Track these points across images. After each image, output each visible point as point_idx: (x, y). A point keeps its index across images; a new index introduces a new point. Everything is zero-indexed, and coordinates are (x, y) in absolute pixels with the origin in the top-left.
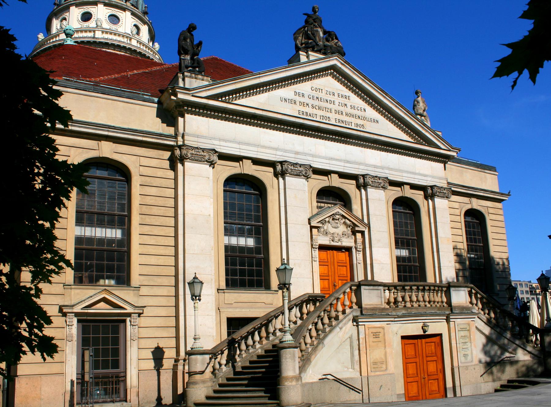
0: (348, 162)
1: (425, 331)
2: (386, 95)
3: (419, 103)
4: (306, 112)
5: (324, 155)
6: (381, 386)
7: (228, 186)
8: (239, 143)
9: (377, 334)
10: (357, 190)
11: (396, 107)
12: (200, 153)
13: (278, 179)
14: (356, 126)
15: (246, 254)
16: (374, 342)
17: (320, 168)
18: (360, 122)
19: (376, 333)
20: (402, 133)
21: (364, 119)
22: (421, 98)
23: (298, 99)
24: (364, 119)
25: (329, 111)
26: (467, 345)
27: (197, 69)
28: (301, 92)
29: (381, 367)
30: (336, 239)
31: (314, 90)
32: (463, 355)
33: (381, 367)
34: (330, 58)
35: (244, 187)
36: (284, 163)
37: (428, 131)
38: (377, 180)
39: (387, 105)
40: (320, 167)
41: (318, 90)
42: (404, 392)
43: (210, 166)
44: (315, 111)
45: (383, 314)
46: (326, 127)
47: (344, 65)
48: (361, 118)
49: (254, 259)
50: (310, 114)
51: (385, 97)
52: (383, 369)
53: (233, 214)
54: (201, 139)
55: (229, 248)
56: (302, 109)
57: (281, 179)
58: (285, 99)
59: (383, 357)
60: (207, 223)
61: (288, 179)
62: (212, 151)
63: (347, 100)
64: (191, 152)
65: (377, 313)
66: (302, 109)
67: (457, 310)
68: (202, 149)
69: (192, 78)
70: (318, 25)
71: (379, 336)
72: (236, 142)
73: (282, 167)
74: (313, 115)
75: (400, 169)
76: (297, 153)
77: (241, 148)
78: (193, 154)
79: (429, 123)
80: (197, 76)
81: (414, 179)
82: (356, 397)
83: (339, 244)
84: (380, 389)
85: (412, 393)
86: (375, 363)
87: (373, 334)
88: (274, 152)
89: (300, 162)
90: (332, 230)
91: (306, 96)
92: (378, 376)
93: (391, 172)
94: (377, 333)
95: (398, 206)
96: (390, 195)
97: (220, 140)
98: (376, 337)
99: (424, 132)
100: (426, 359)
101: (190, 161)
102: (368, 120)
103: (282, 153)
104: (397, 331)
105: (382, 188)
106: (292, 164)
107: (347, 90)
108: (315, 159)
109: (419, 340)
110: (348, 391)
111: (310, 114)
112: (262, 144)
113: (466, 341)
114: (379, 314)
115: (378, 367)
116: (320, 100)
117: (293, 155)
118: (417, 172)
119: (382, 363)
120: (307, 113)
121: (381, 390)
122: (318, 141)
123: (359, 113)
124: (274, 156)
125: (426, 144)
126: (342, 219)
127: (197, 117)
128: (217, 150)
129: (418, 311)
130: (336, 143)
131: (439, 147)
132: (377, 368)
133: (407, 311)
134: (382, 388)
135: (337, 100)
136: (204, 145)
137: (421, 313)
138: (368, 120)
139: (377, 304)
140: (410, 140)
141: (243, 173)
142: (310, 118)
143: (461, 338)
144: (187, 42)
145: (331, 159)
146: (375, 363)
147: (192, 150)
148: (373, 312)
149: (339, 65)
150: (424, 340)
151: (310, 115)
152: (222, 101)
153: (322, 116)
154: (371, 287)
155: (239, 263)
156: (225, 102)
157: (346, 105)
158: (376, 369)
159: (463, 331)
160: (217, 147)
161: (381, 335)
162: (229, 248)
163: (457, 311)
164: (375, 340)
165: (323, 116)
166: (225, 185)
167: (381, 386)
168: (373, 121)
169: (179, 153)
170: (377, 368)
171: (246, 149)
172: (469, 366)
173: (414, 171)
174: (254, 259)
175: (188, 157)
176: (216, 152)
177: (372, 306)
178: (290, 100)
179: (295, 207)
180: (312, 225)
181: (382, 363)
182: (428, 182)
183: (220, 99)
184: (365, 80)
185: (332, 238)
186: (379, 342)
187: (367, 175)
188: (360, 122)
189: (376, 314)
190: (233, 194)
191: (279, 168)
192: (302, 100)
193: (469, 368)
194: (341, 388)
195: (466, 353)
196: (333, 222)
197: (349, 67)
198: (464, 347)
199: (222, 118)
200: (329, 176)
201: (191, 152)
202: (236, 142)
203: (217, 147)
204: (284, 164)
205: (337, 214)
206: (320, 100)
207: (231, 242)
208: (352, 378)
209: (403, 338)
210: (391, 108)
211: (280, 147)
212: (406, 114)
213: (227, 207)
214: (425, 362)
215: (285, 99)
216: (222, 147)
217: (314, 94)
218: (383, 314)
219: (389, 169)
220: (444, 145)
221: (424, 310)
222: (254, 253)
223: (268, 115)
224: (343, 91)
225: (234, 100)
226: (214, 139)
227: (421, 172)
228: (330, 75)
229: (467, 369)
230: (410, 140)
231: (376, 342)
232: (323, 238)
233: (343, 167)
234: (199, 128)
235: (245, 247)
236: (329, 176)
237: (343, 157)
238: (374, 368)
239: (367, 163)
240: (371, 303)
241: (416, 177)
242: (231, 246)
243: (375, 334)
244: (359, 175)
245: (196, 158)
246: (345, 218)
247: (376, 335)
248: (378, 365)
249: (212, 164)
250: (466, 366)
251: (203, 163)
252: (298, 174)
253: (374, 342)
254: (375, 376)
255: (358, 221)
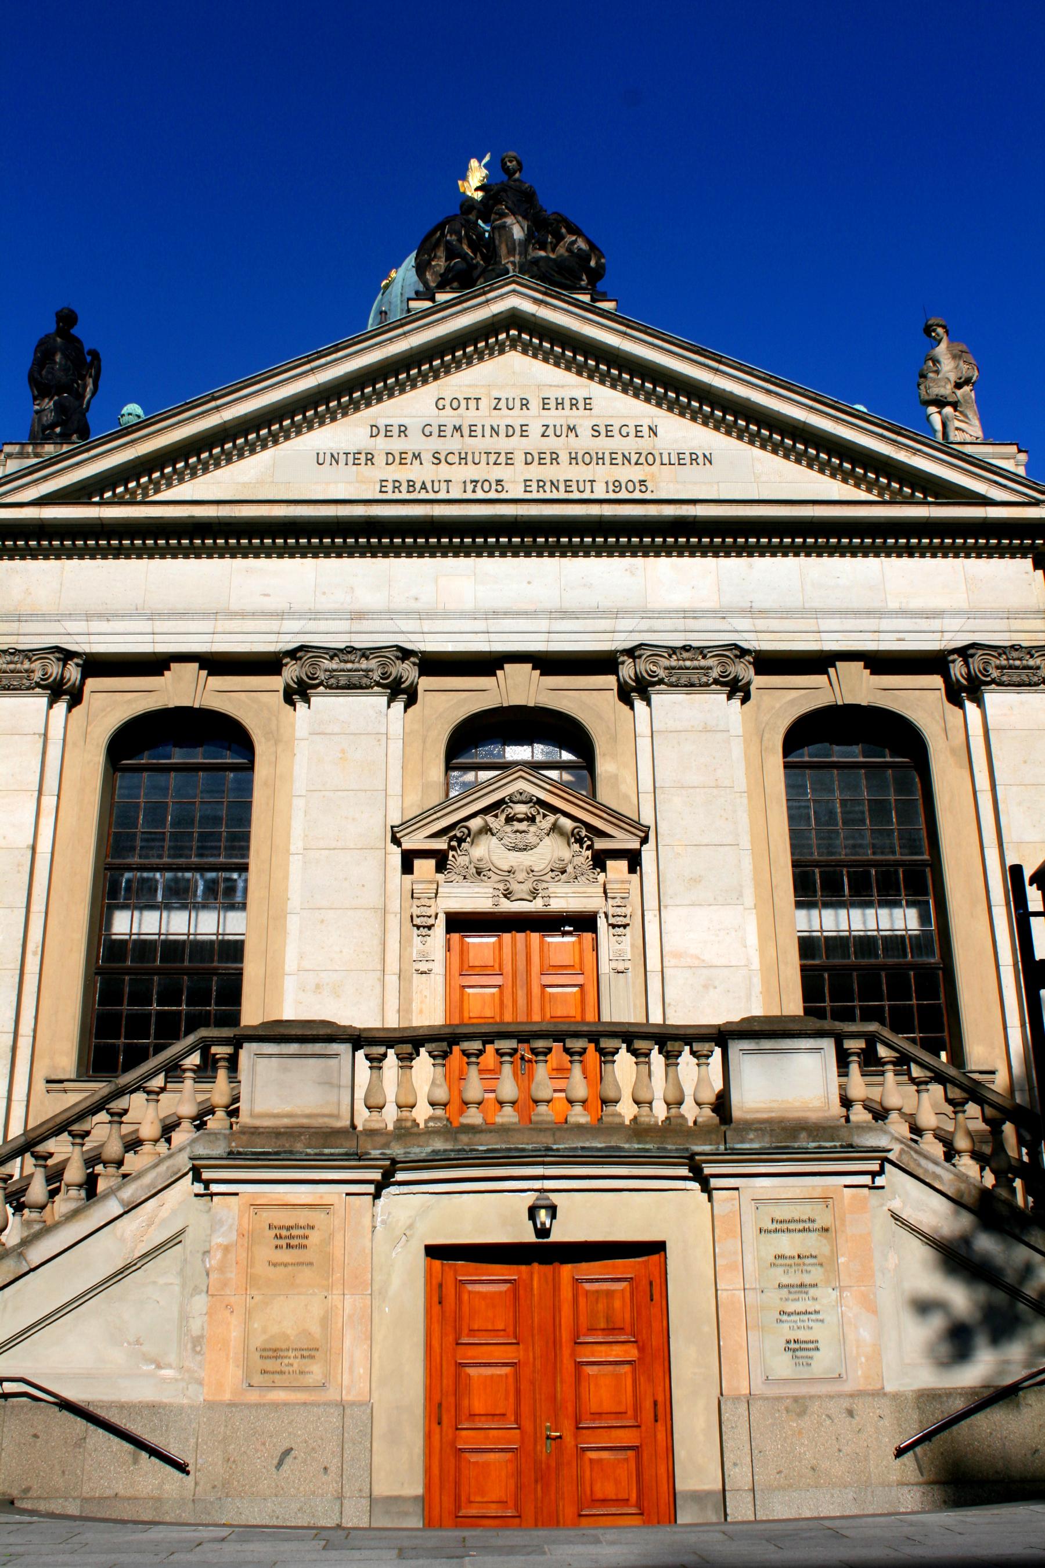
0: (565, 614)
1: (543, 1232)
2: (720, 362)
3: (938, 362)
4: (408, 481)
5: (469, 606)
6: (288, 1452)
7: (146, 753)
8: (152, 617)
9: (294, 1232)
10: (949, 707)
11: (769, 392)
12: (1024, 662)
13: (961, 705)
14: (611, 487)
15: (186, 964)
16: (275, 1265)
17: (450, 649)
18: (636, 473)
19: (288, 1228)
20: (814, 475)
21: (648, 458)
22: (951, 340)
23: (381, 444)
24: (648, 458)
25: (502, 459)
26: (815, 1299)
27: (58, 430)
28: (395, 422)
29: (301, 1373)
30: (521, 889)
31: (448, 407)
32: (784, 1345)
33: (301, 1373)
34: (485, 293)
35: (200, 750)
36: (971, 651)
37: (919, 450)
38: (1020, 659)
39: (731, 393)
40: (450, 647)
41: (463, 403)
42: (419, 1490)
43: (729, 698)
44: (444, 471)
45: (327, 1151)
46: (313, 514)
47: (546, 304)
48: (633, 461)
49: (215, 978)
50: (423, 483)
51: (717, 370)
52: (309, 1380)
53: (153, 840)
54: (30, 623)
55: (130, 946)
56: (396, 473)
57: (970, 707)
58: (332, 456)
59: (315, 1329)
60: (19, 872)
61: (992, 698)
62: (731, 650)
63: (582, 412)
64: (998, 662)
65: (299, 1147)
66: (396, 473)
67: (751, 1136)
68: (24, 651)
69: (28, 458)
70: (507, 207)
71: (304, 1242)
72: (140, 615)
73: (967, 664)
74: (436, 484)
75: (807, 606)
76: (358, 615)
77: (156, 630)
78: (673, 668)
79: (976, 422)
80: (39, 450)
81: (875, 636)
82: (167, 1487)
83: (536, 906)
84: (280, 1464)
85: (478, 1499)
86: (275, 1350)
87: (273, 1232)
88: (274, 625)
89: (361, 642)
90: (506, 859)
91: (414, 432)
92: (276, 1406)
93: (761, 624)
94: (297, 1227)
95: (837, 745)
96: (778, 706)
97: (88, 617)
98: (289, 1246)
99: (902, 456)
100: (573, 1354)
101: (328, 691)
102: (666, 460)
103: (302, 622)
104: (411, 1226)
105: (718, 687)
106: (1000, 651)
107: (584, 381)
108: (427, 626)
109: (536, 1265)
110: (129, 1458)
111: (423, 483)
112: (234, 606)
113: (807, 1279)
114: (309, 1151)
115: (286, 1369)
116: (466, 432)
117: (344, 625)
118: (893, 605)
119: (309, 1353)
120: (411, 484)
121: (285, 1467)
122: (451, 563)
123: (629, 445)
124: (273, 637)
125: (930, 499)
126: (545, 816)
127: (30, 564)
128: (745, 645)
129: (508, 1142)
130: (427, 561)
131: (983, 497)
132: (282, 1373)
133: (456, 1140)
134: (289, 1460)
135: (535, 419)
136: (364, 637)
137: (523, 1150)
138: (666, 460)
139: (318, 1111)
140: (862, 495)
141: (840, 703)
142: (423, 495)
143: (773, 1265)
144: (55, 362)
145: (496, 614)
146: (272, 1352)
147: (670, 656)
148: (279, 1143)
149: (527, 307)
150: (567, 1271)
151: (425, 488)
152: (102, 503)
153: (472, 482)
154: (293, 1048)
155: (158, 994)
156: (121, 502)
157: (571, 429)
158: (277, 1377)
159: (789, 1230)
160: (746, 636)
161: (314, 1237)
162: (130, 946)
163: (751, 1141)
164: (285, 1256)
165: (477, 482)
166: (787, 750)
167: (288, 1452)
168: (688, 461)
169: (964, 670)
170: (282, 1373)
171: (174, 631)
172: (811, 1397)
173: (876, 604)
174: (215, 978)
175: (989, 679)
176: (744, 652)
177: (286, 1121)
178: (351, 457)
179: (340, 793)
180: (406, 846)
181: (309, 1353)
182: (948, 636)
183: (97, 499)
184: (629, 331)
185: (501, 886)
186: (305, 1268)
187: (640, 646)
188: (636, 473)
189: (291, 1152)
190: (160, 778)
191: (958, 669)
192: (397, 445)
193: (815, 1407)
194: (90, 1443)
195: (802, 1335)
196: (508, 829)
197: (565, 306)
198: (791, 1307)
199: (105, 553)
200: (831, 671)
201: (998, 662)
202: (140, 615)
203: (746, 636)
204: (972, 656)
205: (518, 797)
206: (466, 432)
207: (224, 929)
208: (153, 1408)
209: (433, 1252)
210: (748, 400)
211: (296, 607)
212: (811, 408)
213: (138, 818)
214: (568, 1365)
215: (332, 456)
216: (761, 636)
217: (449, 417)
218: (327, 1151)
219: (751, 612)
220: (1005, 486)
221: (544, 1140)
222: (216, 958)
223: (237, 514)
224: (563, 387)
225: (151, 492)
226: (70, 616)
227: (915, 604)
228: (513, 347)
229: (802, 1413)
230: (862, 495)
231: (286, 1265)
232: (465, 890)
233: (544, 637)
234: (30, 594)
235: (184, 941)
236: (831, 671)
237: (553, 604)
238: (264, 1372)
239: (650, 606)
240: (287, 1108)
241: (885, 624)
242: (223, 942)
243: (284, 1233)
244: (279, 653)
245: (1015, 679)
246: (555, 810)
247: (291, 1237)
248: (286, 1361)
249: (737, 689)
250: (796, 1399)
251: (31, 692)
252: (1026, 679)
253: (275, 1265)
254: (258, 1406)
255: (605, 816)
